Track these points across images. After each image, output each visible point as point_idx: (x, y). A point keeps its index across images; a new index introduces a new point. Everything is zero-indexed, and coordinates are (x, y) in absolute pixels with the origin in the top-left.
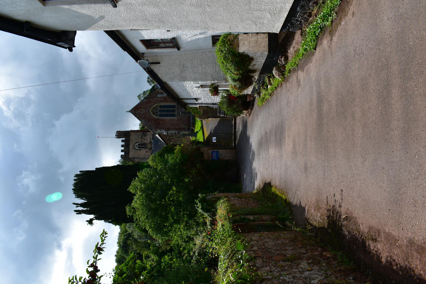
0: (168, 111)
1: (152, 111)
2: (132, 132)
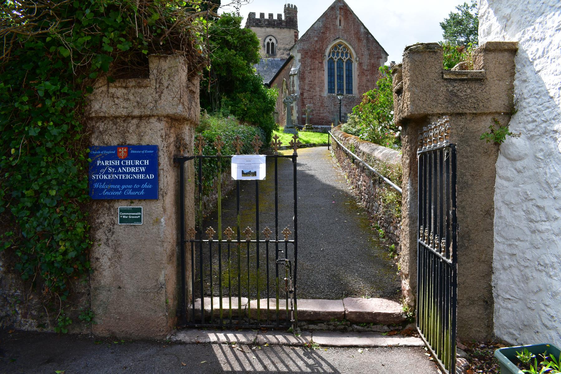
0: (340, 77)
1: (340, 45)
2: (295, 32)
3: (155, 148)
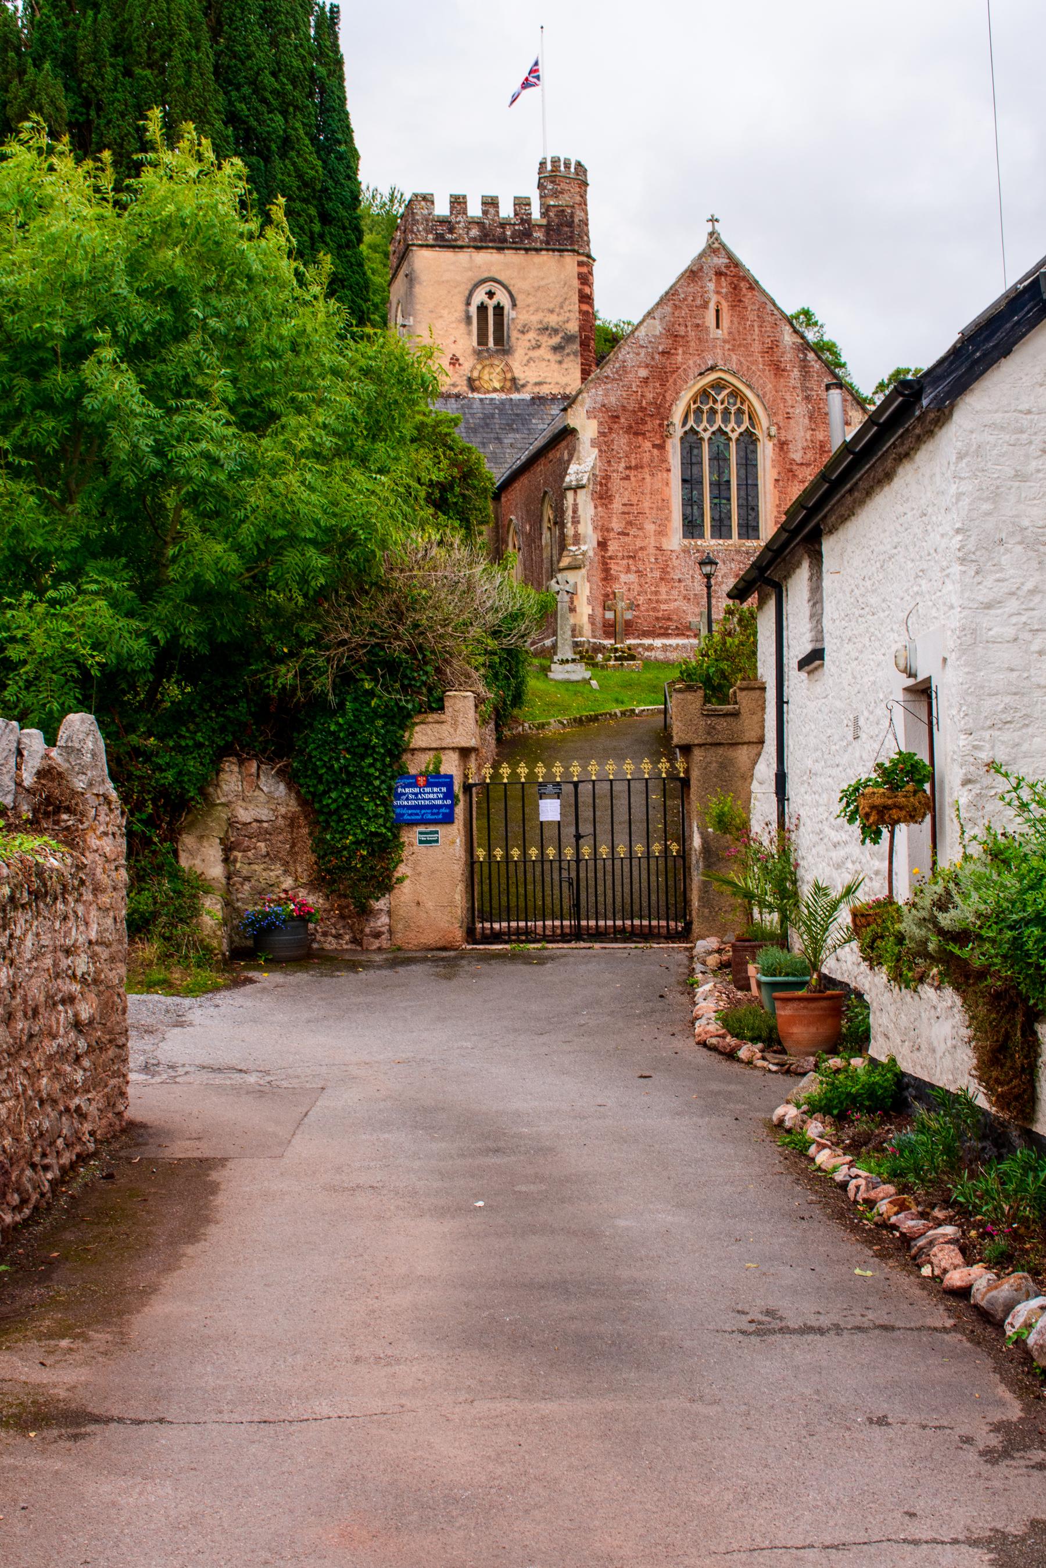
1: (718, 385)
2: (580, 264)
3: (451, 777)
